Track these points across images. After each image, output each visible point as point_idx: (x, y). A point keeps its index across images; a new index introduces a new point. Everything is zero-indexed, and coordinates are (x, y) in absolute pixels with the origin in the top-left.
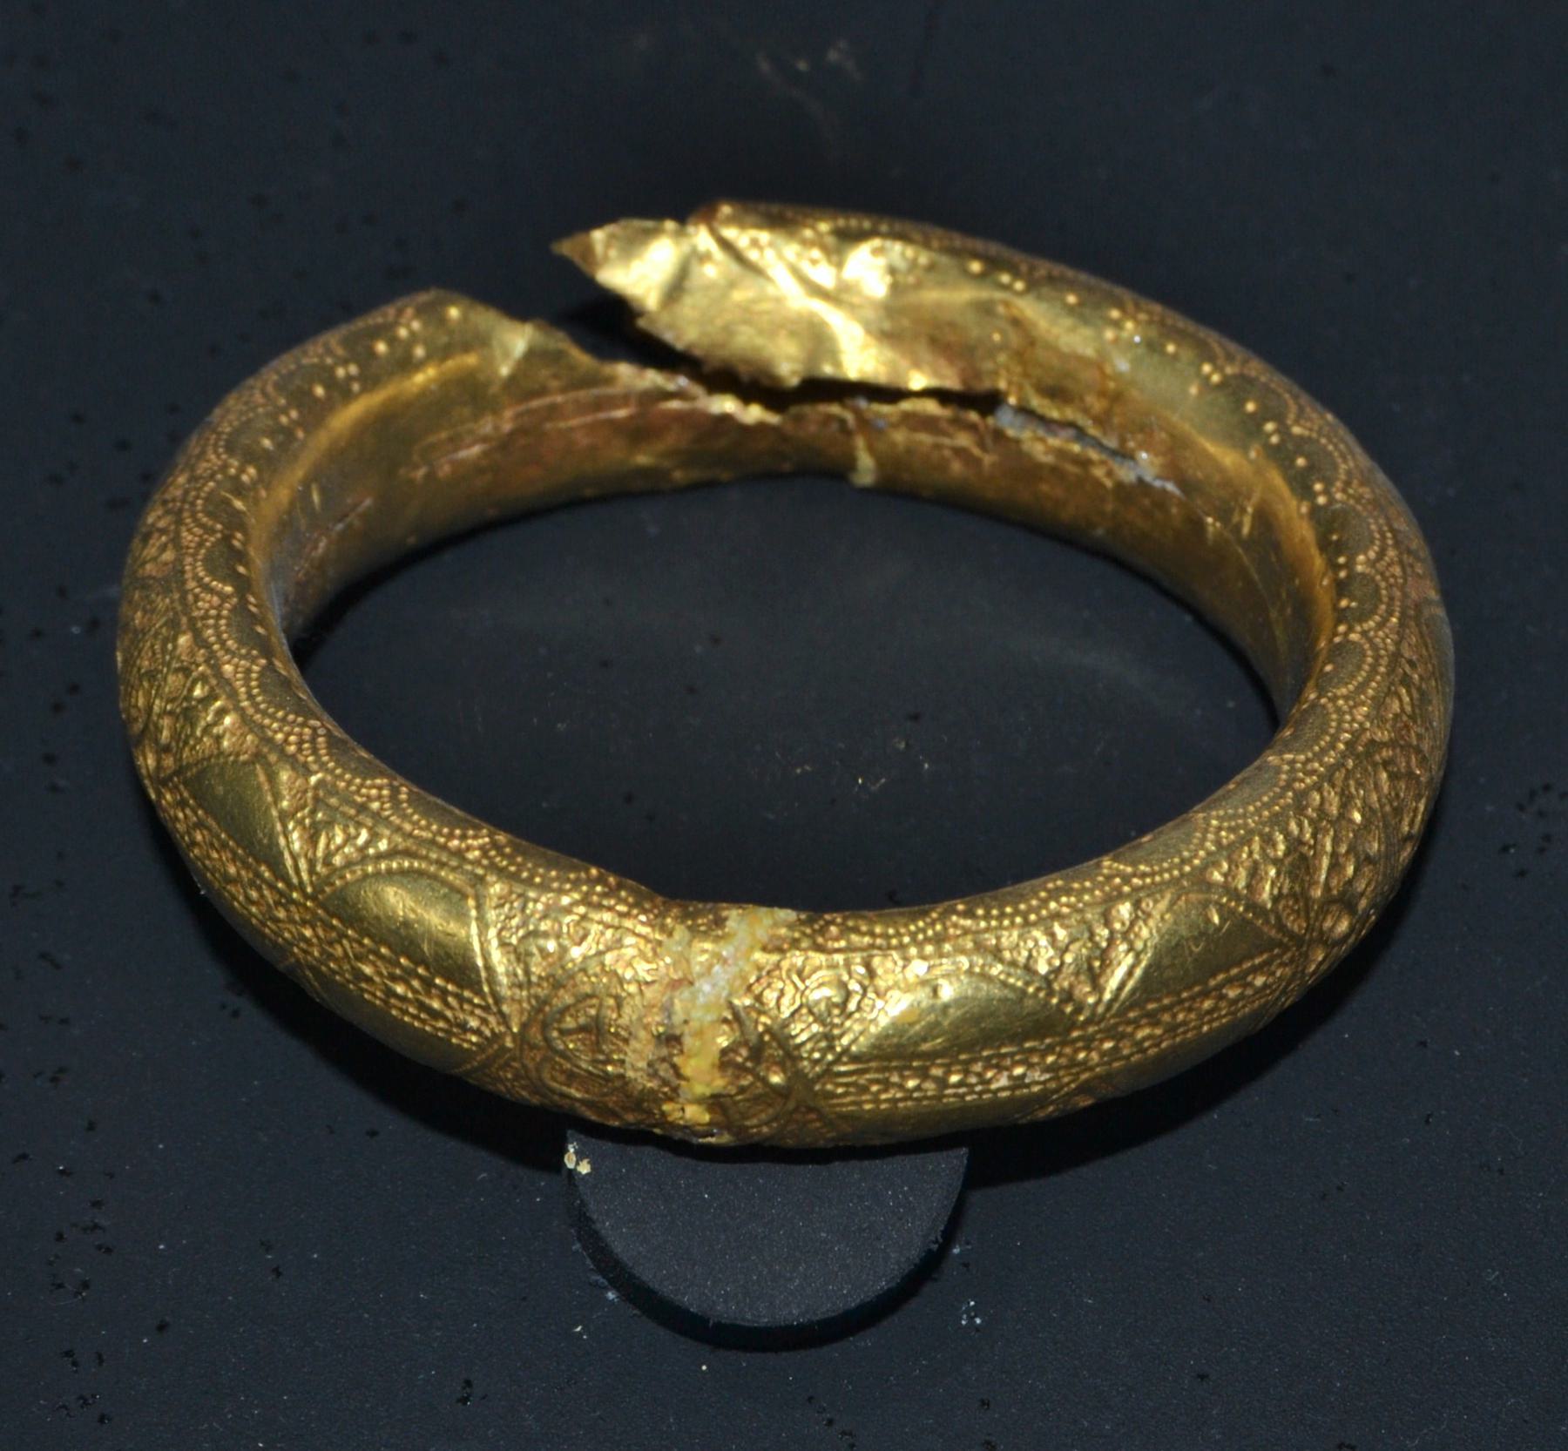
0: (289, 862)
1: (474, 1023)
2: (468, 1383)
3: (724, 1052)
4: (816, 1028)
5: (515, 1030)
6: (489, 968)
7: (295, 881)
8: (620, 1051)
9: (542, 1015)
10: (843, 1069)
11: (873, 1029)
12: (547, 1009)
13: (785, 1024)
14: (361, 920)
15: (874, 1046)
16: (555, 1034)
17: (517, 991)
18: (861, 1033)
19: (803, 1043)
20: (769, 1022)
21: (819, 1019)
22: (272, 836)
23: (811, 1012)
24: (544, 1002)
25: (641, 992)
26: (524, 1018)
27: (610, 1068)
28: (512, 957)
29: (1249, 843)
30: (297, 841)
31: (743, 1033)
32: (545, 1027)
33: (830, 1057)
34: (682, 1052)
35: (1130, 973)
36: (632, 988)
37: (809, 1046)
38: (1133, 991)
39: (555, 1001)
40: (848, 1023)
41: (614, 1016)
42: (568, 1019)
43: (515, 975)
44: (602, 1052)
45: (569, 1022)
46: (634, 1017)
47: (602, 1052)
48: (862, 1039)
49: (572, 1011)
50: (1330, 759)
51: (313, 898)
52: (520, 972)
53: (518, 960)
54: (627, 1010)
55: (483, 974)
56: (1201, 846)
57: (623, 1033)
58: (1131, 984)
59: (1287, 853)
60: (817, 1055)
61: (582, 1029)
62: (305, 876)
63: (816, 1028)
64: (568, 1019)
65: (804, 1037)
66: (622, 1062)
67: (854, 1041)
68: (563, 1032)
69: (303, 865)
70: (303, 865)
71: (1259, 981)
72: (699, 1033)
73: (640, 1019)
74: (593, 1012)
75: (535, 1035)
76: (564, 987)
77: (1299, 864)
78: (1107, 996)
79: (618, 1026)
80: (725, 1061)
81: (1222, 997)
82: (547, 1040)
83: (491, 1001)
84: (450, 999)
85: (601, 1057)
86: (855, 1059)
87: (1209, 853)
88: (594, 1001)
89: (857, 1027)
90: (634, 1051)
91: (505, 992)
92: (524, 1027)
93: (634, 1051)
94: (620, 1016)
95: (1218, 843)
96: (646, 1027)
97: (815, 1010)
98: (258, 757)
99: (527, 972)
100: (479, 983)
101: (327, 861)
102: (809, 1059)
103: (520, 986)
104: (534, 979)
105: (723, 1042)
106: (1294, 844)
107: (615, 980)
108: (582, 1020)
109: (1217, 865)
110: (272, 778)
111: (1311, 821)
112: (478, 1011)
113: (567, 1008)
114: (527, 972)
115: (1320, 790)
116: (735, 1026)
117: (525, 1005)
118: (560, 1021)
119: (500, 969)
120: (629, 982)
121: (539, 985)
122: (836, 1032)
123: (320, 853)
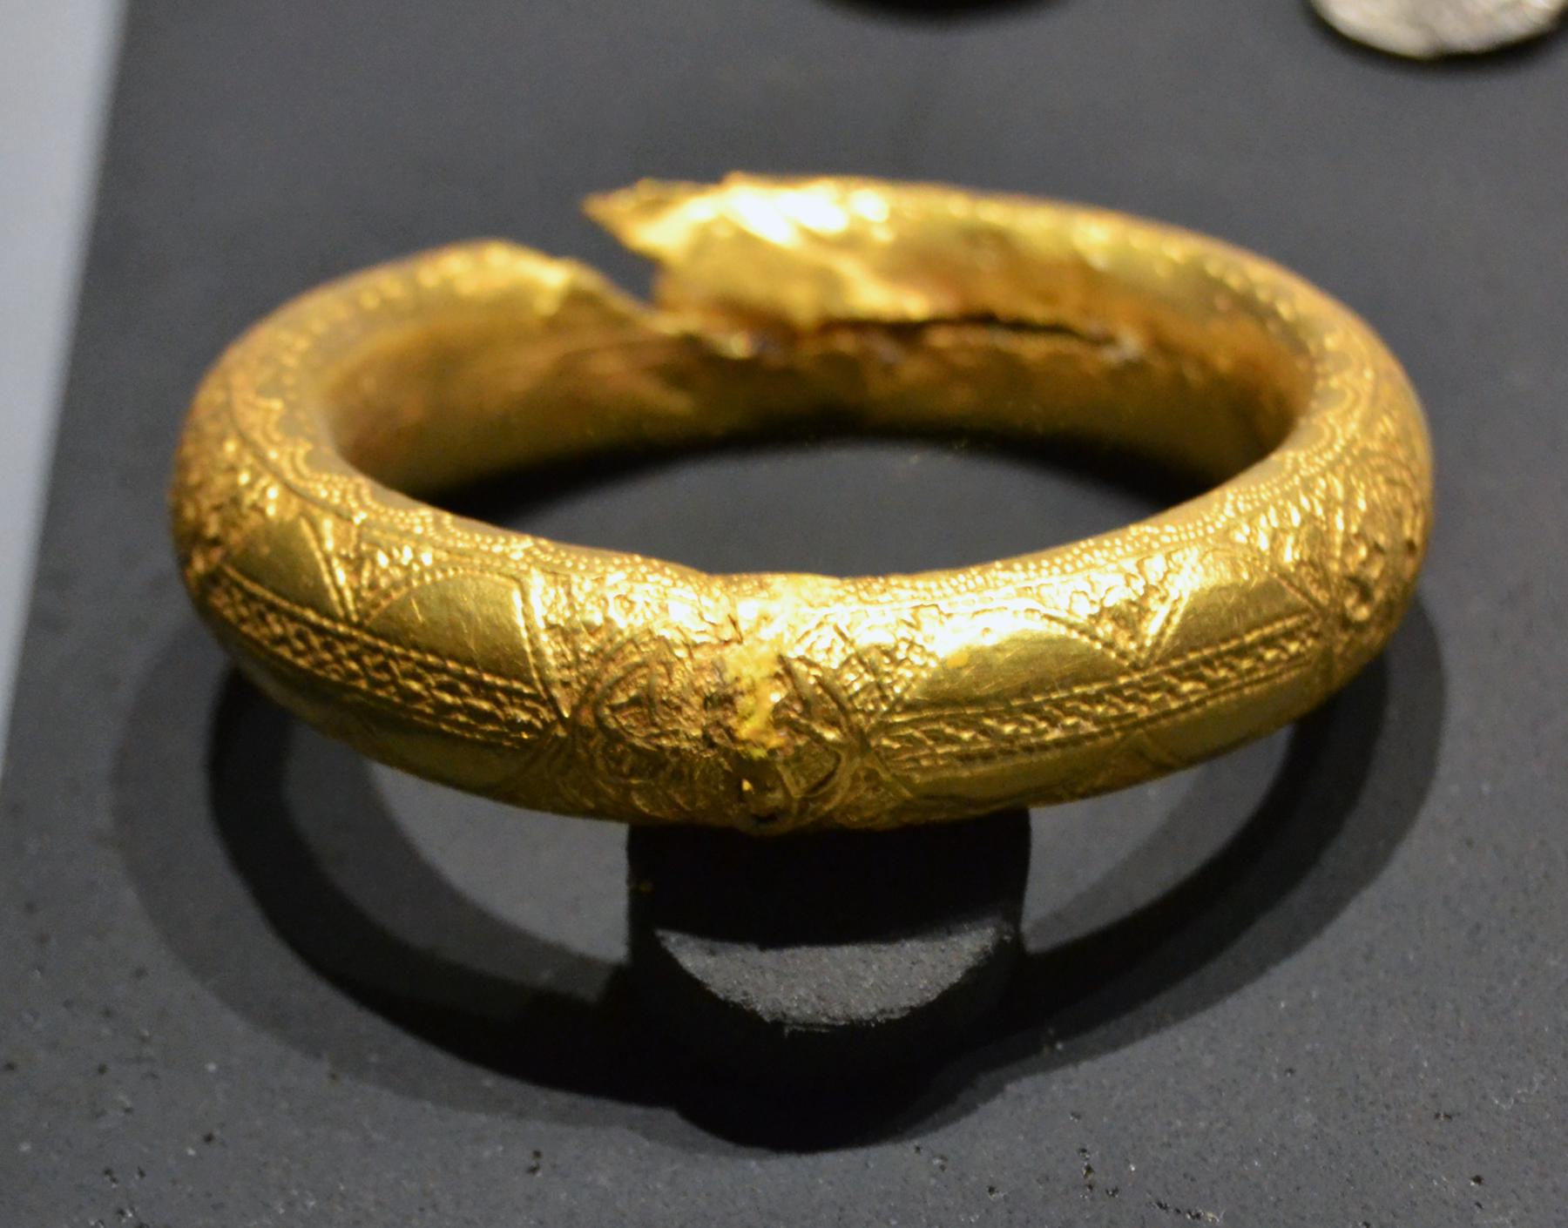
0: (334, 596)
1: (524, 717)
2: (537, 1154)
3: (777, 708)
4: (869, 678)
5: (566, 715)
6: (538, 653)
7: (340, 612)
8: (674, 721)
9: (591, 696)
10: (898, 719)
11: (924, 675)
12: (598, 687)
13: (837, 675)
14: (406, 631)
15: (925, 693)
16: (607, 712)
17: (566, 672)
18: (913, 680)
19: (857, 694)
20: (819, 674)
21: (872, 669)
22: (317, 577)
23: (861, 662)
24: (596, 678)
25: (691, 656)
26: (575, 701)
27: (664, 742)
28: (560, 639)
29: (1265, 512)
30: (342, 576)
31: (795, 687)
32: (596, 706)
33: (884, 708)
34: (735, 712)
35: (1168, 621)
36: (681, 653)
37: (862, 697)
38: (1175, 636)
39: (605, 677)
40: (901, 671)
41: (666, 683)
42: (619, 694)
43: (564, 655)
44: (655, 725)
45: (621, 698)
46: (686, 682)
47: (655, 725)
48: (914, 686)
49: (623, 685)
50: (1329, 456)
51: (359, 626)
52: (568, 653)
53: (566, 640)
54: (677, 676)
55: (532, 660)
56: (1221, 511)
57: (676, 701)
58: (1170, 631)
59: (1303, 523)
60: (871, 707)
61: (635, 702)
62: (351, 607)
63: (869, 678)
64: (619, 694)
65: (857, 687)
66: (676, 733)
67: (907, 689)
68: (614, 709)
69: (348, 595)
70: (348, 595)
71: (1293, 647)
72: (753, 690)
73: (691, 683)
74: (643, 682)
75: (586, 717)
76: (613, 660)
77: (1317, 537)
78: (1148, 643)
79: (671, 693)
80: (778, 719)
81: (1260, 658)
82: (599, 721)
83: (540, 687)
84: (500, 695)
85: (656, 731)
86: (910, 707)
87: (1229, 519)
88: (645, 671)
89: (909, 674)
90: (688, 719)
91: (554, 675)
92: (575, 710)
93: (688, 719)
94: (671, 682)
95: (1237, 511)
96: (697, 691)
97: (866, 660)
98: (304, 514)
99: (575, 652)
100: (528, 670)
101: (373, 586)
102: (863, 711)
103: (569, 667)
104: (583, 656)
105: (776, 697)
106: (1309, 518)
107: (663, 645)
108: (633, 693)
109: (1237, 526)
110: (314, 526)
111: (1321, 501)
112: (528, 703)
113: (618, 681)
114: (575, 652)
115: (1324, 476)
116: (788, 680)
117: (575, 686)
118: (609, 697)
119: (549, 651)
120: (677, 646)
121: (588, 662)
122: (887, 680)
123: (365, 582)
